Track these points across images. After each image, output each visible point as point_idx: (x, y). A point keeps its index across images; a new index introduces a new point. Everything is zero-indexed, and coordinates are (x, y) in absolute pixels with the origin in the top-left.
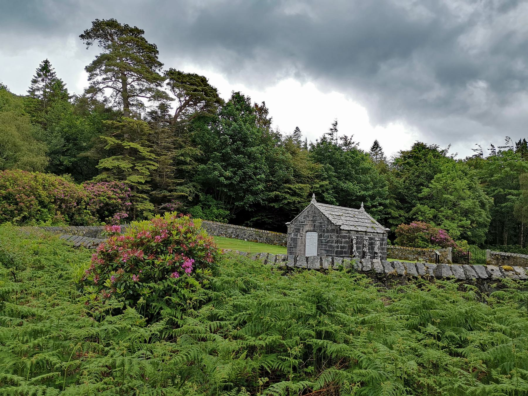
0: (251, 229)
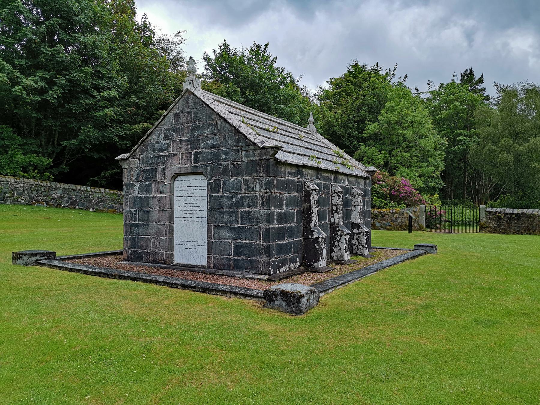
0: (102, 190)
